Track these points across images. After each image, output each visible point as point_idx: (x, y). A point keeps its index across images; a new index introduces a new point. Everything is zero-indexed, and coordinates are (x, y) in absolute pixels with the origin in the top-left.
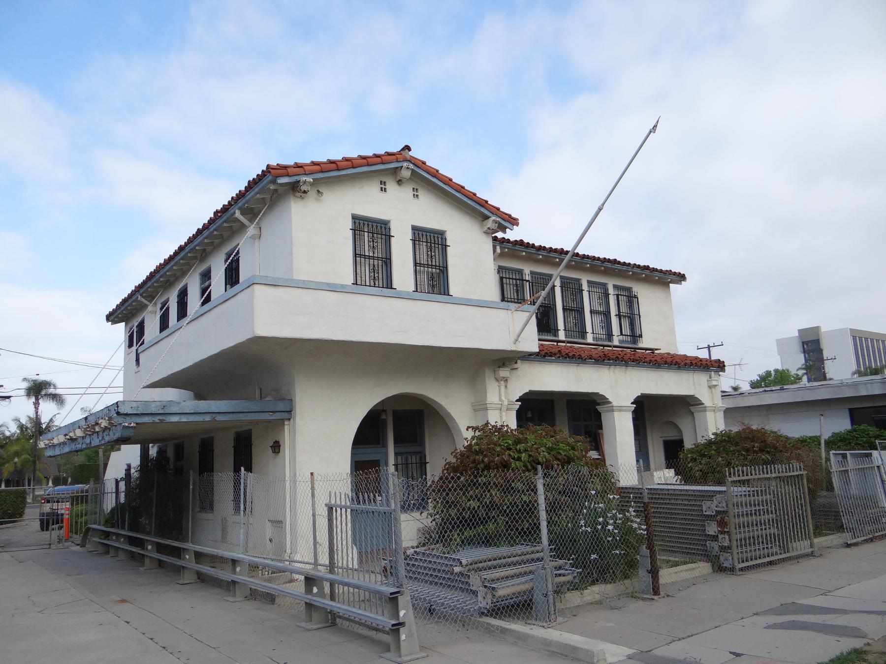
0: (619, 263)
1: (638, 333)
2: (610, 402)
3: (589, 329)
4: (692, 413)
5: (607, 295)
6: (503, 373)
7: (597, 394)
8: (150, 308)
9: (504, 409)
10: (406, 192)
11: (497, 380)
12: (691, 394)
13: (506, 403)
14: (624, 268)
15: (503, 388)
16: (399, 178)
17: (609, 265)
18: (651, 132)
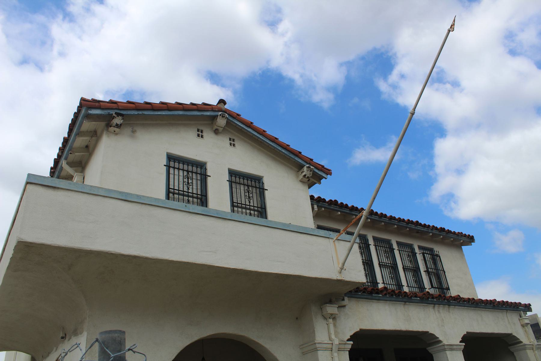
0: (420, 224)
1: (445, 286)
2: (440, 342)
3: (404, 283)
4: (512, 354)
5: (414, 254)
6: (331, 309)
7: (426, 333)
10: (223, 141)
11: (325, 318)
12: (509, 332)
13: (336, 342)
14: (425, 229)
15: (331, 326)
16: (215, 127)
17: (413, 226)
18: (449, 31)
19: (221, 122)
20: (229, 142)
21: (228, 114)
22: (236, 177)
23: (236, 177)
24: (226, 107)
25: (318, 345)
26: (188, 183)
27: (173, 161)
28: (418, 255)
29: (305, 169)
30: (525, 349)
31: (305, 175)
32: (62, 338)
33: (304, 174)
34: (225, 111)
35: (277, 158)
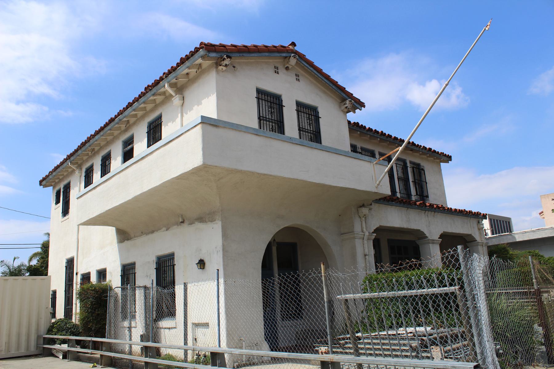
1: (425, 194)
2: (427, 237)
3: (398, 190)
6: (365, 211)
8: (77, 172)
9: (366, 238)
12: (470, 233)
19: (293, 61)
20: (295, 77)
21: (299, 56)
22: (301, 107)
23: (301, 107)
24: (296, 48)
25: (356, 235)
26: (272, 112)
27: (262, 95)
28: (409, 168)
29: (348, 102)
30: (477, 245)
31: (346, 107)
32: (182, 222)
33: (346, 106)
34: (296, 53)
35: (317, 84)
